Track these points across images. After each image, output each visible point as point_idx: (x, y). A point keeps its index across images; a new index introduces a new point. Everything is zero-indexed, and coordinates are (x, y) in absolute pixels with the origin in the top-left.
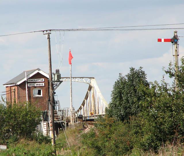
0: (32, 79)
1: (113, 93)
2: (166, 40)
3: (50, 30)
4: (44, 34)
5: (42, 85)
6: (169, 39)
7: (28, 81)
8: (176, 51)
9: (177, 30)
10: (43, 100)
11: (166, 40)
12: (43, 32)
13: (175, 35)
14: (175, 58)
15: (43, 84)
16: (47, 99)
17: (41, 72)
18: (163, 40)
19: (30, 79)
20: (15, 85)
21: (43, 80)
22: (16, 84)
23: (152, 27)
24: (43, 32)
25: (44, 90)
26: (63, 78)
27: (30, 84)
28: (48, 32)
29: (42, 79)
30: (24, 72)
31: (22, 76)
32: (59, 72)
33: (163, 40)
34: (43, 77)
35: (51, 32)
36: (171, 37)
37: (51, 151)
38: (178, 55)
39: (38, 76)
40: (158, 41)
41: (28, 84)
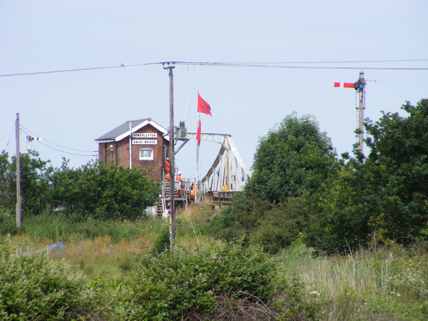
0: (139, 134)
1: (255, 157)
2: (346, 85)
3: (174, 63)
4: (165, 68)
5: (153, 144)
6: (352, 84)
7: (133, 137)
8: (361, 101)
9: (364, 71)
10: (155, 165)
11: (346, 85)
12: (163, 64)
13: (360, 78)
14: (358, 112)
15: (156, 141)
16: (160, 165)
17: (152, 123)
18: (342, 85)
19: (135, 134)
20: (113, 141)
21: (155, 135)
22: (114, 140)
23: (340, 65)
24: (163, 64)
25: (156, 150)
26: (189, 133)
27: (154, 137)
28: (171, 65)
30: (128, 122)
31: (124, 127)
32: (184, 126)
33: (342, 85)
34: (154, 129)
35: (175, 65)
36: (354, 80)
38: (364, 108)
39: (149, 128)
41: (133, 141)
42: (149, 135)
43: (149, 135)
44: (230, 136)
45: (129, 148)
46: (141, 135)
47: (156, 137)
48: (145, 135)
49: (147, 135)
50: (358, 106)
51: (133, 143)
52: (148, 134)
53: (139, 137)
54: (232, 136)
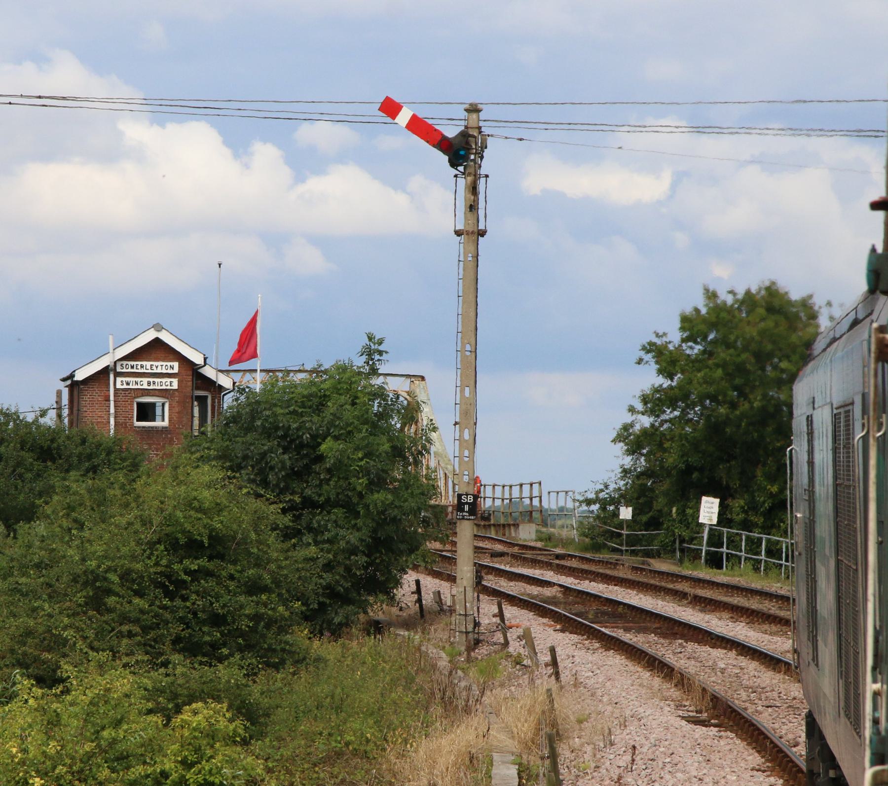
0: (133, 363)
2: (417, 126)
7: (119, 369)
17: (166, 337)
18: (404, 117)
19: (125, 363)
21: (172, 368)
27: (124, 379)
29: (169, 364)
33: (404, 117)
37: (624, 706)
38: (482, 233)
40: (380, 109)
41: (119, 380)
42: (157, 367)
43: (157, 367)
44: (423, 378)
45: (109, 396)
46: (139, 367)
47: (176, 370)
48: (147, 365)
49: (154, 368)
50: (460, 227)
51: (119, 386)
52: (159, 363)
53: (134, 370)
54: (426, 378)
